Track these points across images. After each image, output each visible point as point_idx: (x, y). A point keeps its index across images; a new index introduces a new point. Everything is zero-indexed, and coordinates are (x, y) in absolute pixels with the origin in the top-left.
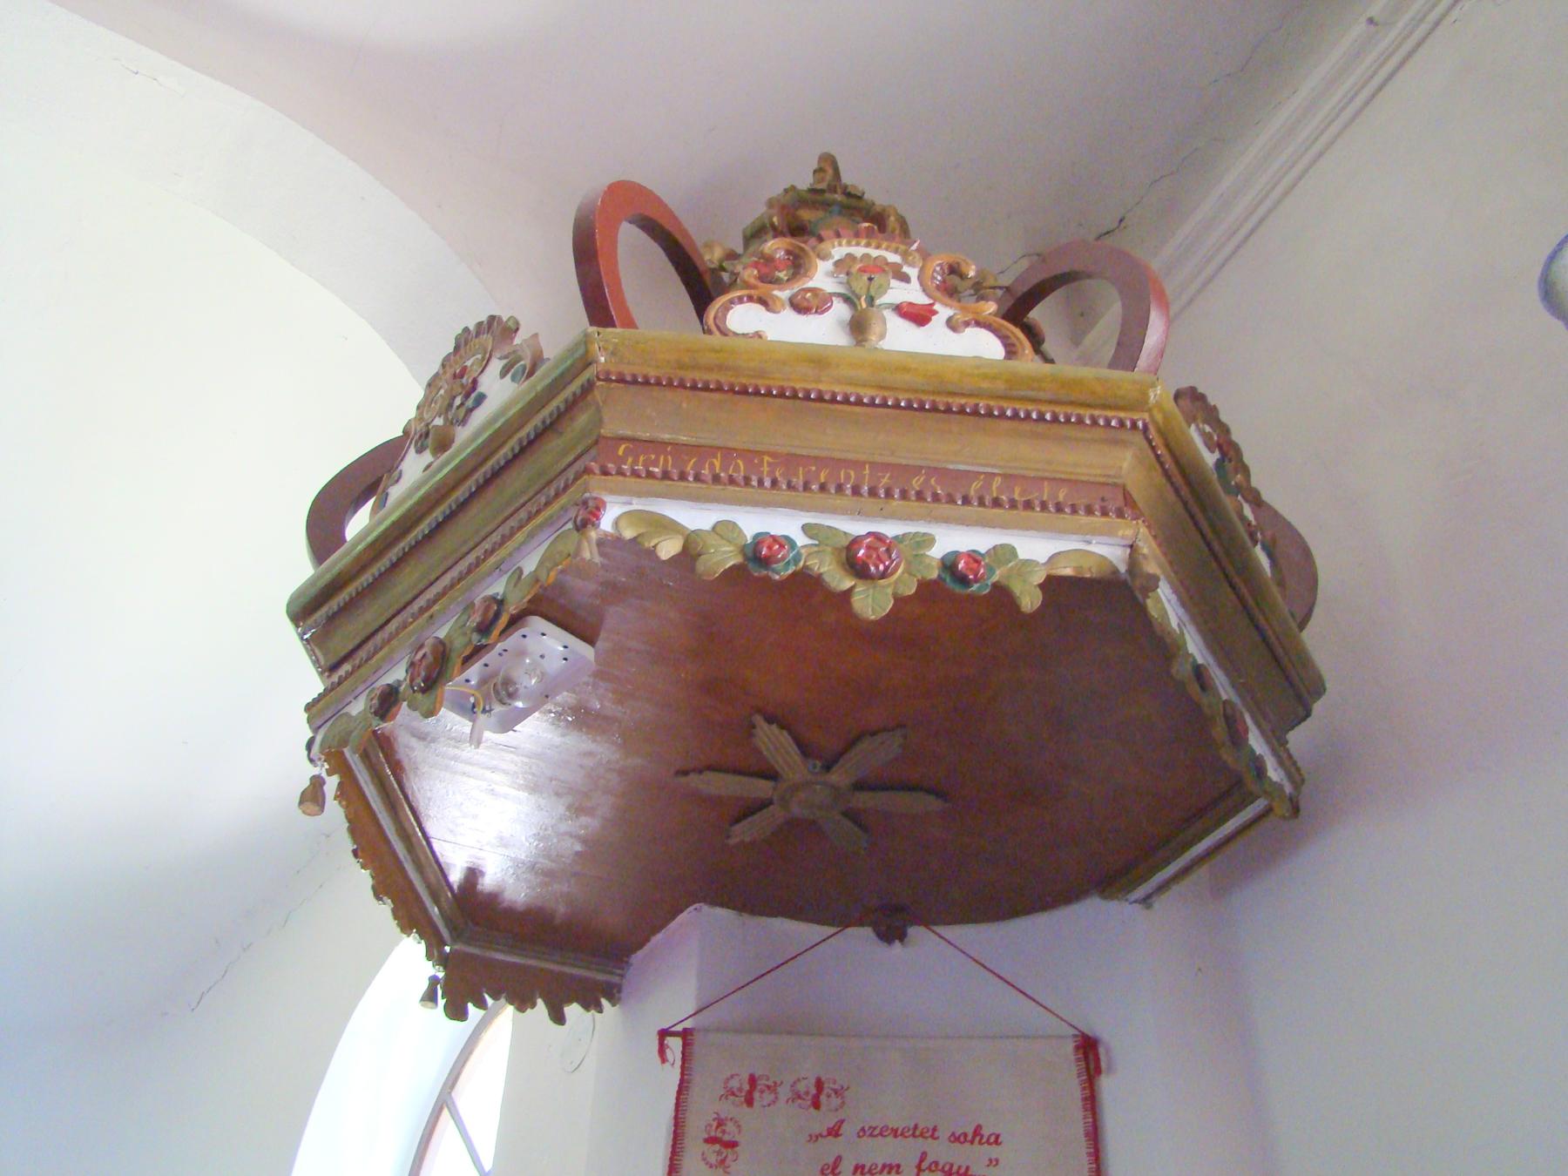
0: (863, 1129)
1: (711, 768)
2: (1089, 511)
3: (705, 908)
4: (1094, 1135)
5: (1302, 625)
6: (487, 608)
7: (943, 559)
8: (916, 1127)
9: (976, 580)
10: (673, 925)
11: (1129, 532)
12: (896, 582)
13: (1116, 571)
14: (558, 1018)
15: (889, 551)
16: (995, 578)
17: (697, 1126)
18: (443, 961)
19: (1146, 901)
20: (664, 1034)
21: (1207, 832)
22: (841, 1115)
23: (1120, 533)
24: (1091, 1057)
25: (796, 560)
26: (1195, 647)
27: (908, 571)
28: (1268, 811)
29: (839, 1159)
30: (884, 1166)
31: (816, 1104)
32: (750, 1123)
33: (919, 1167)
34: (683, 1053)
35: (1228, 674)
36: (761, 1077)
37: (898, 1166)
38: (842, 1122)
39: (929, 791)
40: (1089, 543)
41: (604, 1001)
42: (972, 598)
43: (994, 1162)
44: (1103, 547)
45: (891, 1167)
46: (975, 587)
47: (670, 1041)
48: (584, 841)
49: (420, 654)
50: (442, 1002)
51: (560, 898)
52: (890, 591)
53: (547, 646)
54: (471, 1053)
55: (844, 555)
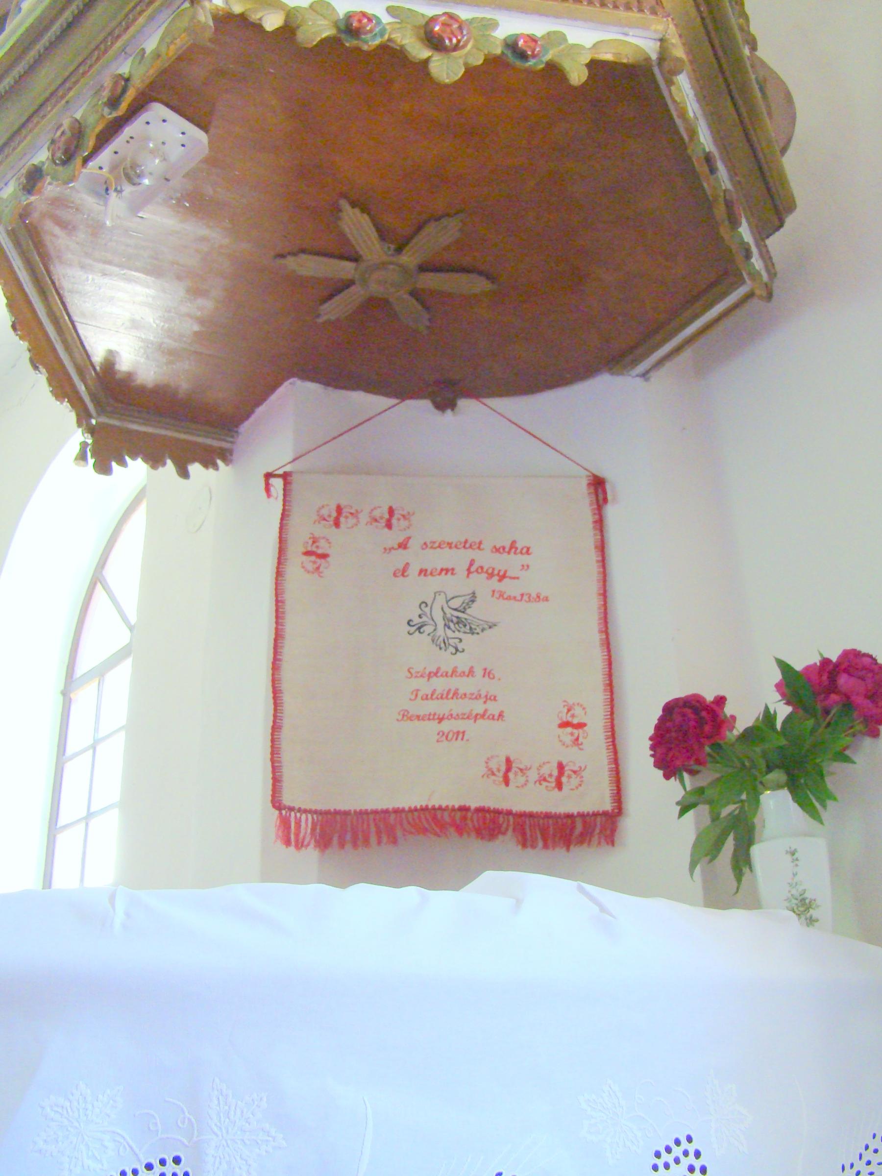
0: (425, 544)
1: (303, 251)
2: (628, 8)
3: (298, 382)
4: (602, 548)
5: (784, 150)
6: (116, 84)
7: (505, 40)
8: (466, 542)
9: (534, 56)
10: (273, 397)
11: (660, 27)
12: (468, 53)
13: (648, 59)
14: (184, 473)
15: (460, 28)
16: (548, 57)
17: (295, 549)
18: (92, 431)
19: (645, 375)
20: (268, 476)
21: (696, 316)
22: (408, 533)
23: (653, 27)
24: (600, 491)
25: (382, 34)
26: (705, 139)
27: (476, 47)
28: (750, 296)
29: (407, 565)
30: (442, 570)
31: (389, 526)
32: (338, 541)
33: (469, 570)
34: (285, 490)
35: (728, 171)
36: (346, 506)
37: (453, 569)
38: (409, 538)
39: (481, 273)
40: (626, 35)
41: (220, 463)
42: (529, 71)
43: (526, 567)
44: (634, 38)
45: (447, 571)
46: (531, 62)
47: (273, 481)
48: (201, 321)
49: (59, 133)
50: (91, 461)
51: (182, 376)
52: (461, 61)
53: (167, 137)
54: (115, 541)
55: (422, 32)
